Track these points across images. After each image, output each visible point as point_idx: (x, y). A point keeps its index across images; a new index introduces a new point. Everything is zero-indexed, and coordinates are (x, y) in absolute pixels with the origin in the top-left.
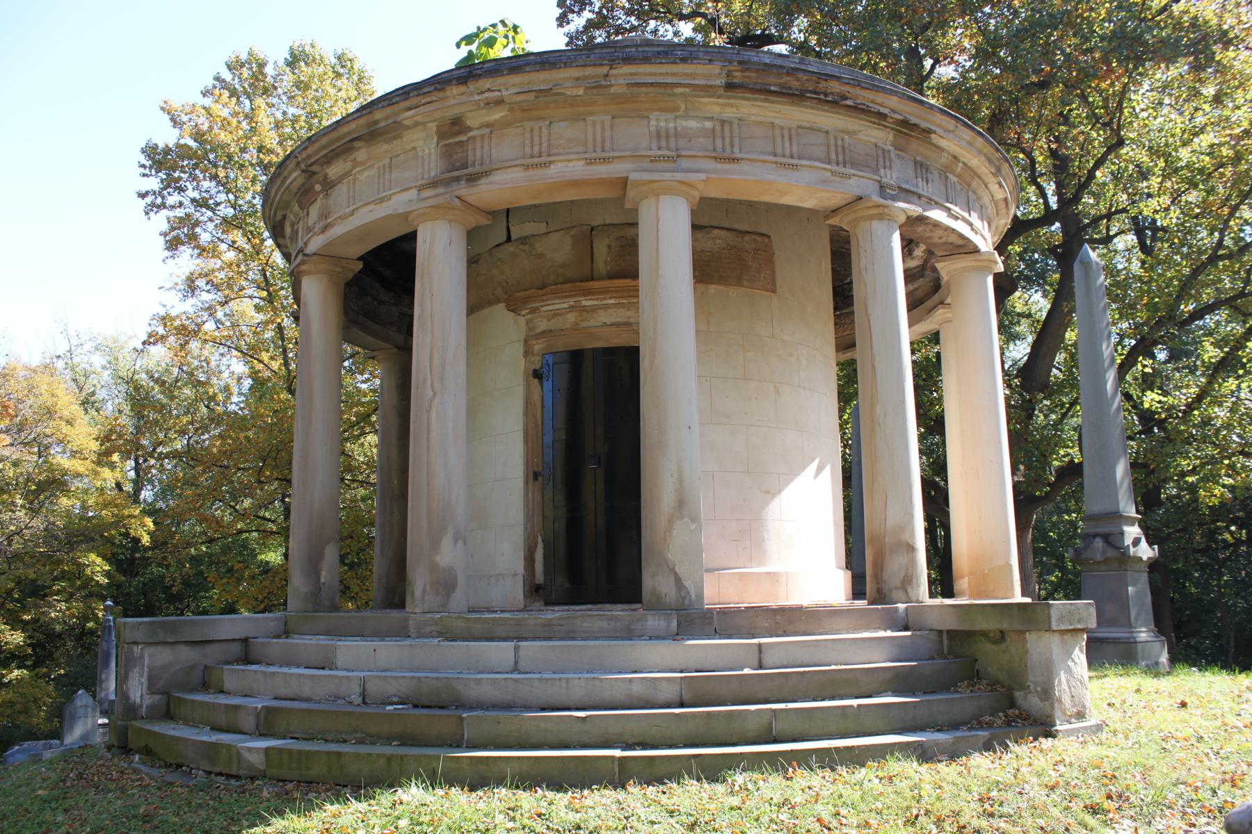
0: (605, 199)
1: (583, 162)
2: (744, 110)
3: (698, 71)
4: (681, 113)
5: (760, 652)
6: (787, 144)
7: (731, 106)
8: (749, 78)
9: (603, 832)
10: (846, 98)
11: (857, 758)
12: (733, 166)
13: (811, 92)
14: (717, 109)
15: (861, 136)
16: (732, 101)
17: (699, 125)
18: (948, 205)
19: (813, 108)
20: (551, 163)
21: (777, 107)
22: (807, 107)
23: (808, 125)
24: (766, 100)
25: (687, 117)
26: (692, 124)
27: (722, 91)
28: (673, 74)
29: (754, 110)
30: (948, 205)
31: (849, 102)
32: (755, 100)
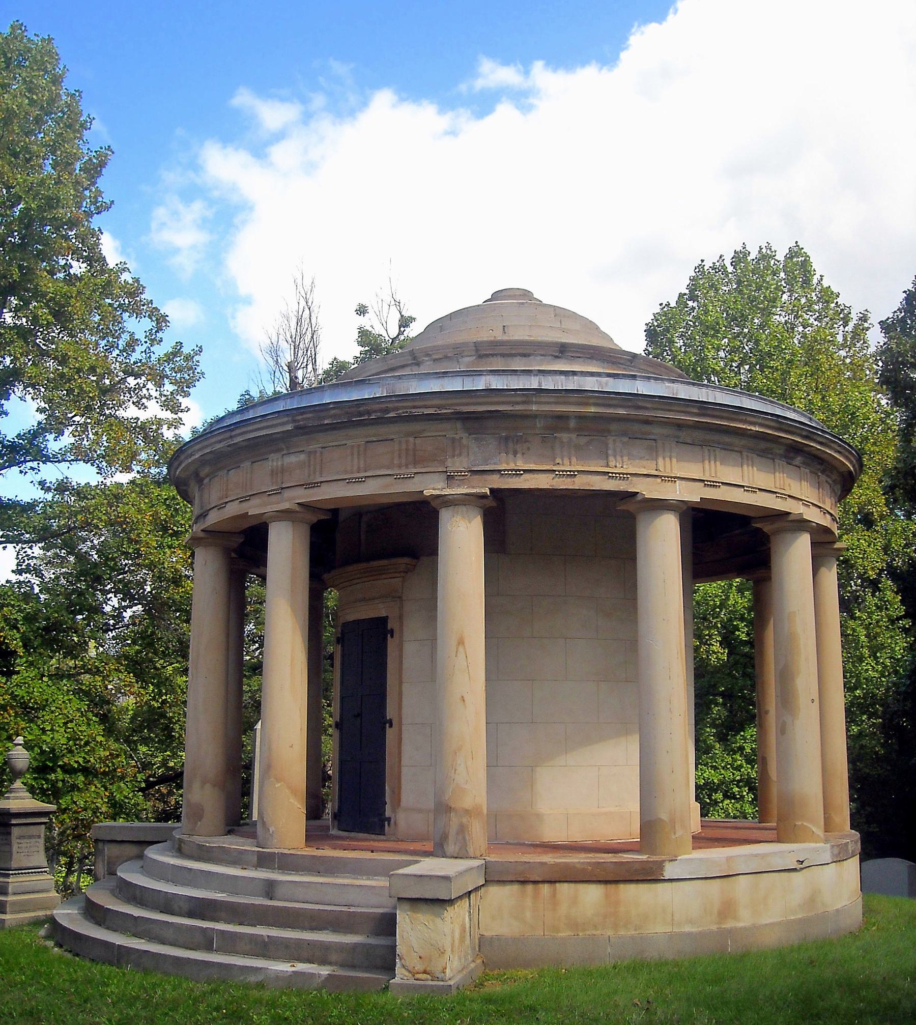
6: (356, 461)
17: (297, 459)
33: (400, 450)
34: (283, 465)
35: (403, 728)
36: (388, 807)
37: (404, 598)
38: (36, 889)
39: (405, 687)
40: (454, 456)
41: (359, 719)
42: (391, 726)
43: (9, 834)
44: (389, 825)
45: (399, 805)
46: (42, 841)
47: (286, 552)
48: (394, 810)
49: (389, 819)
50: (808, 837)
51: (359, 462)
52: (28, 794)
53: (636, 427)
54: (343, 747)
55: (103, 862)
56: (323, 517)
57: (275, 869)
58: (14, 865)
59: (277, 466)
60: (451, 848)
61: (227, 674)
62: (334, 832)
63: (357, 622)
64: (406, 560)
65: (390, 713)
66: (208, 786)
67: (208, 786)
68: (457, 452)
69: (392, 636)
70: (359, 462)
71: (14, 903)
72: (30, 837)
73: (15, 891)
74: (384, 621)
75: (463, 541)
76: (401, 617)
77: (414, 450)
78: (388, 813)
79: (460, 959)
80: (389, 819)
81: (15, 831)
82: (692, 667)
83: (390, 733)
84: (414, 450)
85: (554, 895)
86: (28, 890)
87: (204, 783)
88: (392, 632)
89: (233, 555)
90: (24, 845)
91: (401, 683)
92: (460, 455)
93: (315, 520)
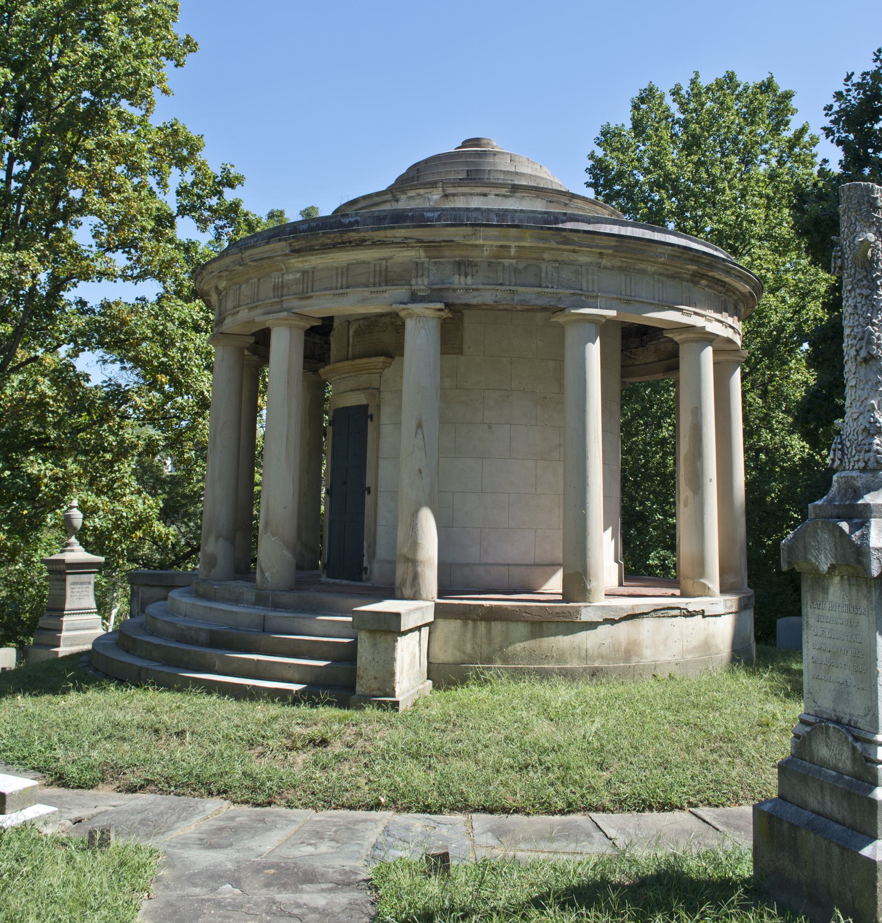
1: (247, 310)
5: (264, 620)
6: (340, 279)
9: (437, 921)
10: (366, 241)
11: (254, 695)
12: (308, 302)
13: (340, 243)
14: (300, 265)
18: (642, 266)
20: (454, 195)
21: (331, 255)
23: (354, 262)
24: (323, 253)
26: (291, 277)
28: (266, 252)
29: (319, 261)
30: (642, 266)
33: (375, 271)
34: (282, 282)
36: (365, 558)
38: (86, 626)
39: (382, 463)
40: (417, 277)
42: (369, 493)
43: (65, 580)
45: (374, 557)
46: (92, 587)
47: (284, 348)
48: (370, 562)
49: (366, 569)
50: (705, 592)
52: (81, 547)
54: (331, 508)
56: (315, 324)
57: (268, 606)
58: (67, 606)
60: (407, 592)
61: (239, 449)
62: (324, 579)
64: (382, 359)
65: (369, 482)
66: (221, 540)
68: (420, 273)
69: (371, 420)
71: (67, 638)
72: (82, 583)
74: (365, 407)
75: (420, 336)
76: (379, 407)
77: (386, 271)
78: (366, 564)
79: (475, 684)
80: (366, 569)
81: (70, 579)
82: (617, 467)
83: (368, 499)
84: (386, 271)
85: (489, 631)
86: (78, 627)
87: (217, 538)
88: (371, 417)
89: (246, 352)
90: (77, 590)
91: (378, 458)
92: (422, 275)
93: (309, 326)
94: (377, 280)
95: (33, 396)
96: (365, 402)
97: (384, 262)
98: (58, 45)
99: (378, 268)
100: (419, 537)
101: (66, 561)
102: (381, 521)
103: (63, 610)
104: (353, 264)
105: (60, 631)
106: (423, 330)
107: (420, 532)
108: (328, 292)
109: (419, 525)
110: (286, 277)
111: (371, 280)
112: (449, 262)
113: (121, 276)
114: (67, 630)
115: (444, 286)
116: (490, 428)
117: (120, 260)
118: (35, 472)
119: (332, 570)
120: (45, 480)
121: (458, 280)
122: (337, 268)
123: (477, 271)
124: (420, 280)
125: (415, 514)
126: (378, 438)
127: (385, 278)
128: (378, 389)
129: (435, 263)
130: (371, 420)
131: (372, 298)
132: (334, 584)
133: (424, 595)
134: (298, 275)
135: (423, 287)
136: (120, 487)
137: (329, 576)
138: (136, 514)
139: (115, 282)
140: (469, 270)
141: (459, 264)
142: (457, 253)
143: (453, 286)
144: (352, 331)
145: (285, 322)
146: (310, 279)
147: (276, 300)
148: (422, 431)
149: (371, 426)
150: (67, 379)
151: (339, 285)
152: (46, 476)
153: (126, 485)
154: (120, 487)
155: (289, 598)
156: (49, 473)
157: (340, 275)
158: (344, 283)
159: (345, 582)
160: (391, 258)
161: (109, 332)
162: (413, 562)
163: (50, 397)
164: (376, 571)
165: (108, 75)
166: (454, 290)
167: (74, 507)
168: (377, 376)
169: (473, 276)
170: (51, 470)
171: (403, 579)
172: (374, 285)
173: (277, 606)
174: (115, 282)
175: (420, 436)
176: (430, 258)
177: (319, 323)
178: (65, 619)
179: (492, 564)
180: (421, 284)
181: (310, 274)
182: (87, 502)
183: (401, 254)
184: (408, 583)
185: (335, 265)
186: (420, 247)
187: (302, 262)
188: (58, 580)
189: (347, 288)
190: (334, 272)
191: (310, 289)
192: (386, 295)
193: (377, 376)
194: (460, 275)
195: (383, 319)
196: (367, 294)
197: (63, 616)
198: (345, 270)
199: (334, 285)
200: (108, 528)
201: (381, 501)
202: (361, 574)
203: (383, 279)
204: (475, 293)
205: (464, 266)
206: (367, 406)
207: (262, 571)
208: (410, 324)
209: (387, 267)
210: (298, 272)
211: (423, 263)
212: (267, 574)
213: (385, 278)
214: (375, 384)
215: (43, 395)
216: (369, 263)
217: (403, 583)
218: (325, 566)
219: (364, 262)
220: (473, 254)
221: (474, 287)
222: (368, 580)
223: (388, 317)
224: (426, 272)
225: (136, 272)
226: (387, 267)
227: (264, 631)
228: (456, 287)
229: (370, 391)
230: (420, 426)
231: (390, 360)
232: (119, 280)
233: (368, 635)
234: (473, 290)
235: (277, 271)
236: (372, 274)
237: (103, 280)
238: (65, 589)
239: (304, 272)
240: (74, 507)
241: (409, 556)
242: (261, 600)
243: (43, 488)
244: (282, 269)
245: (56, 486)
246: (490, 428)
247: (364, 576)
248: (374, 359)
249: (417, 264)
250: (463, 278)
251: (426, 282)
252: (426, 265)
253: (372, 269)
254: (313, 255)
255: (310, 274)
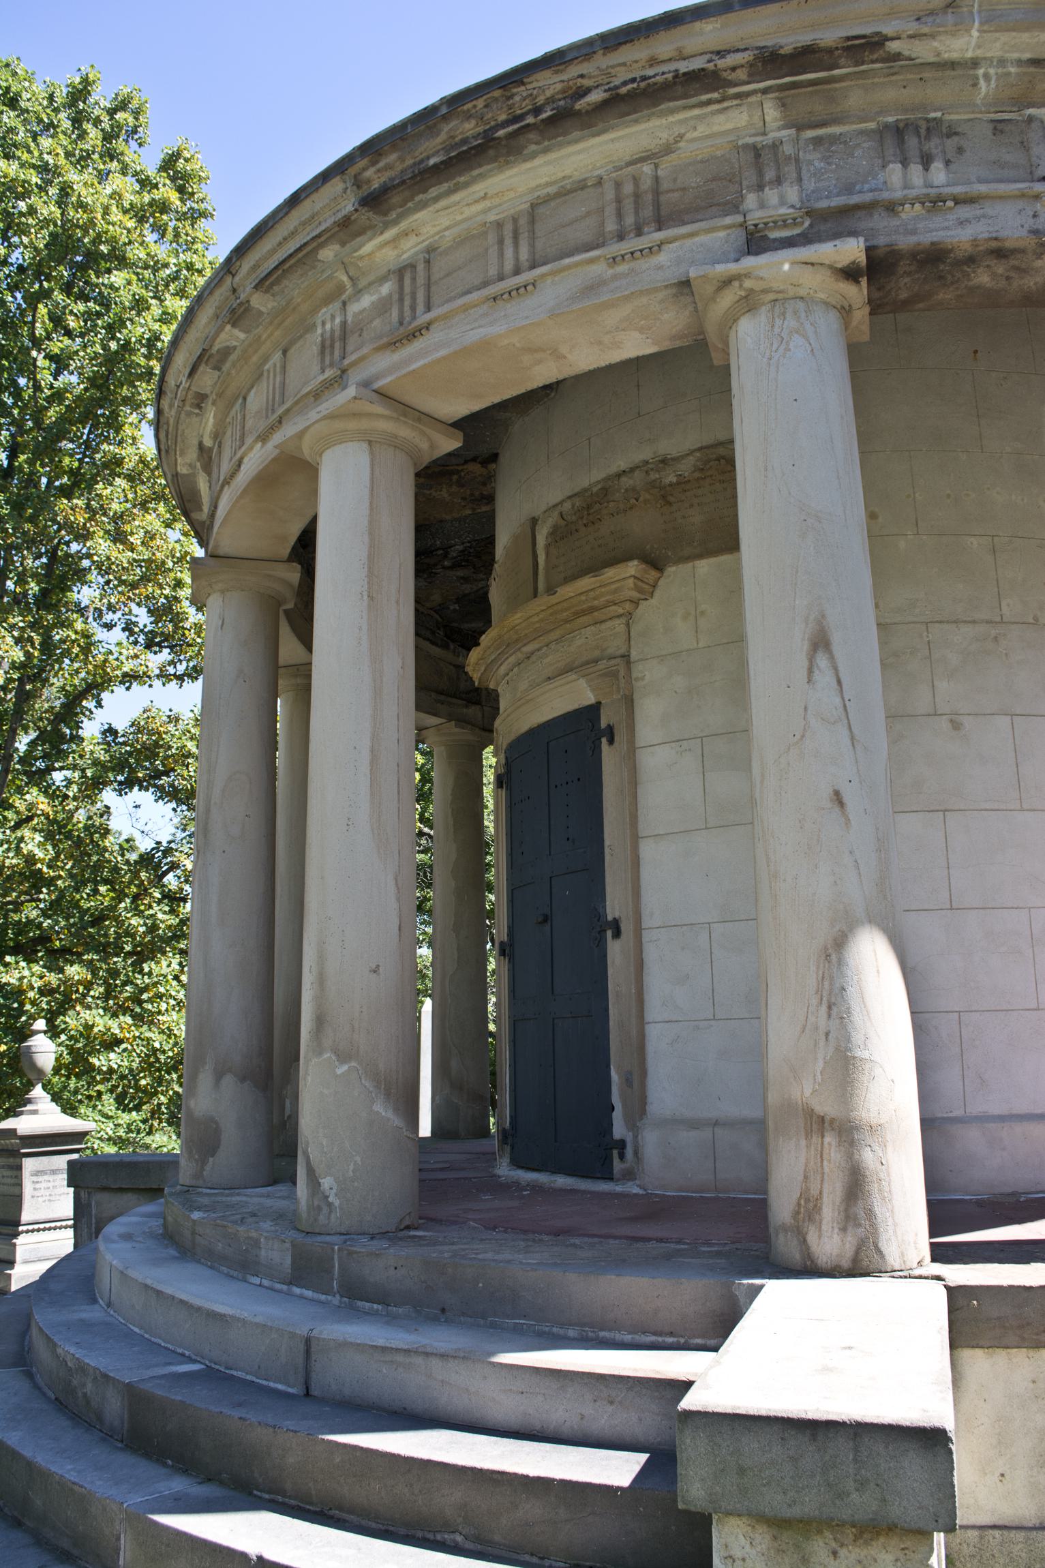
0: (681, 348)
2: (428, 231)
3: (318, 206)
4: (349, 291)
5: (308, 1352)
6: (509, 252)
7: (406, 234)
8: (389, 167)
10: (584, 92)
15: (151, 294)
16: (404, 225)
17: (374, 298)
19: (546, 151)
21: (479, 188)
22: (533, 156)
23: (552, 190)
25: (358, 293)
26: (367, 301)
27: (366, 216)
28: (293, 234)
31: (596, 97)
32: (436, 199)
33: (619, 201)
34: (344, 324)
35: (646, 936)
36: (618, 1117)
37: (634, 654)
39: (647, 850)
40: (760, 187)
41: (547, 927)
42: (617, 934)
43: (19, 1168)
44: (622, 1157)
45: (643, 1112)
49: (622, 1145)
51: (516, 252)
53: (400, 1358)
55: (89, 1228)
58: (25, 1217)
59: (332, 331)
62: (504, 1170)
63: (534, 733)
64: (633, 568)
65: (614, 907)
66: (229, 1080)
67: (228, 1080)
68: (770, 174)
69: (611, 742)
70: (516, 252)
73: (27, 1257)
77: (657, 192)
78: (619, 1130)
80: (622, 1145)
81: (29, 1165)
83: (615, 950)
84: (657, 192)
87: (219, 1076)
88: (610, 733)
91: (635, 839)
92: (779, 181)
94: (630, 220)
95: (14, 861)
96: (589, 698)
97: (647, 169)
98: (43, 322)
99: (628, 188)
100: (857, 1038)
101: (20, 1133)
102: (655, 1009)
103: (18, 1224)
104: (548, 199)
105: (11, 1263)
106: (797, 340)
107: (857, 1017)
108: (475, 296)
109: (852, 992)
110: (354, 308)
111: (611, 226)
112: (862, 132)
113: (158, 676)
114: (26, 1262)
115: (855, 199)
116: (956, 726)
117: (156, 660)
118: (13, 981)
119: (524, 1145)
120: (31, 994)
121: (896, 179)
122: (499, 225)
123: (960, 150)
124: (772, 195)
125: (835, 950)
126: (634, 782)
127: (654, 208)
128: (626, 657)
129: (818, 141)
130: (611, 742)
131: (615, 277)
132: (536, 1188)
133: (893, 1257)
134: (386, 289)
135: (783, 211)
136: (150, 1000)
137: (517, 1163)
138: (176, 1044)
139: (151, 686)
140: (933, 145)
141: (899, 132)
142: (890, 95)
143: (885, 195)
144: (541, 541)
145: (352, 425)
146: (421, 280)
147: (329, 373)
148: (832, 658)
149: (609, 756)
150: (83, 846)
151: (509, 266)
152: (32, 988)
153: (160, 996)
154: (150, 1000)
155: (390, 1265)
156: (37, 983)
157: (508, 242)
158: (524, 255)
159: (562, 1181)
160: (668, 150)
161: (140, 761)
162: (843, 1130)
163: (42, 861)
164: (663, 1148)
165: (113, 345)
166: (891, 208)
167: (38, 1032)
168: (619, 625)
169: (948, 163)
170: (41, 978)
171: (805, 1196)
172: (621, 237)
173: (359, 1296)
174: (151, 686)
175: (824, 678)
176: (800, 128)
177: (450, 444)
178: (20, 1240)
179: (1001, 1118)
180: (775, 204)
181: (421, 267)
182: (93, 1026)
183: (702, 130)
184: (829, 1212)
185: (492, 217)
186: (765, 91)
187: (394, 241)
188: (11, 1167)
189: (533, 266)
190: (492, 238)
191: (420, 308)
192: (663, 258)
193: (619, 625)
194: (905, 163)
195: (624, 479)
196: (599, 269)
197: (16, 1235)
198: (523, 221)
199: (493, 271)
200: (131, 1070)
201: (651, 953)
202: (608, 1160)
203: (648, 212)
204: (964, 212)
205: (910, 136)
206: (595, 709)
207: (311, 1172)
208: (749, 335)
209: (657, 179)
210: (383, 279)
211: (775, 146)
212: (327, 1183)
213: (654, 208)
214: (615, 646)
215: (30, 859)
216: (600, 182)
217: (809, 1209)
218: (505, 1135)
219: (582, 185)
220: (941, 98)
221: (958, 190)
222: (629, 1175)
223: (637, 473)
224: (790, 170)
225: (181, 668)
226: (657, 179)
227: (307, 1394)
228: (898, 194)
229: (602, 665)
230: (820, 642)
231: (654, 574)
232: (157, 683)
233: (763, 1537)
234: (958, 201)
235: (327, 300)
236: (610, 210)
237: (135, 684)
238: (20, 1185)
239: (401, 272)
240: (38, 1032)
241: (826, 1107)
242: (307, 1271)
243: (28, 1007)
244: (341, 288)
245: (48, 1003)
246: (956, 726)
247: (617, 1166)
248: (610, 573)
249: (756, 151)
250: (916, 170)
251: (792, 194)
252: (788, 149)
253: (610, 194)
254: (423, 205)
255: (421, 267)
